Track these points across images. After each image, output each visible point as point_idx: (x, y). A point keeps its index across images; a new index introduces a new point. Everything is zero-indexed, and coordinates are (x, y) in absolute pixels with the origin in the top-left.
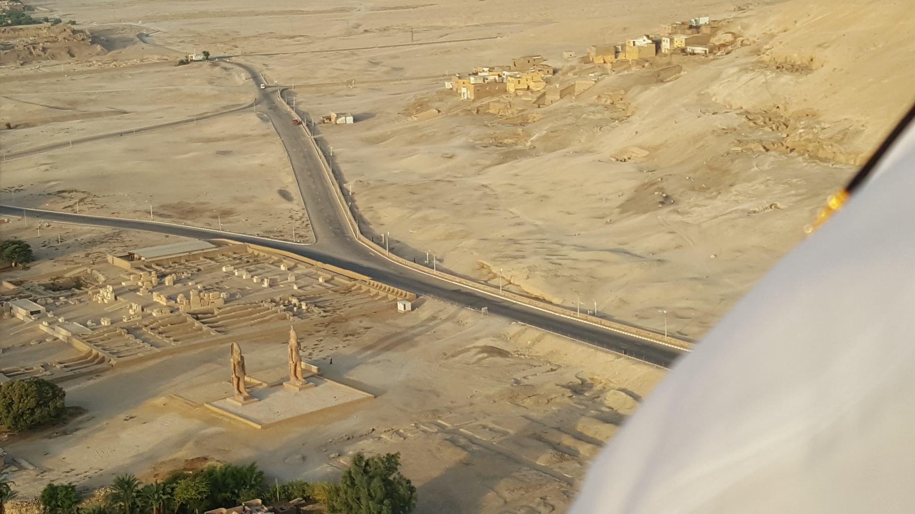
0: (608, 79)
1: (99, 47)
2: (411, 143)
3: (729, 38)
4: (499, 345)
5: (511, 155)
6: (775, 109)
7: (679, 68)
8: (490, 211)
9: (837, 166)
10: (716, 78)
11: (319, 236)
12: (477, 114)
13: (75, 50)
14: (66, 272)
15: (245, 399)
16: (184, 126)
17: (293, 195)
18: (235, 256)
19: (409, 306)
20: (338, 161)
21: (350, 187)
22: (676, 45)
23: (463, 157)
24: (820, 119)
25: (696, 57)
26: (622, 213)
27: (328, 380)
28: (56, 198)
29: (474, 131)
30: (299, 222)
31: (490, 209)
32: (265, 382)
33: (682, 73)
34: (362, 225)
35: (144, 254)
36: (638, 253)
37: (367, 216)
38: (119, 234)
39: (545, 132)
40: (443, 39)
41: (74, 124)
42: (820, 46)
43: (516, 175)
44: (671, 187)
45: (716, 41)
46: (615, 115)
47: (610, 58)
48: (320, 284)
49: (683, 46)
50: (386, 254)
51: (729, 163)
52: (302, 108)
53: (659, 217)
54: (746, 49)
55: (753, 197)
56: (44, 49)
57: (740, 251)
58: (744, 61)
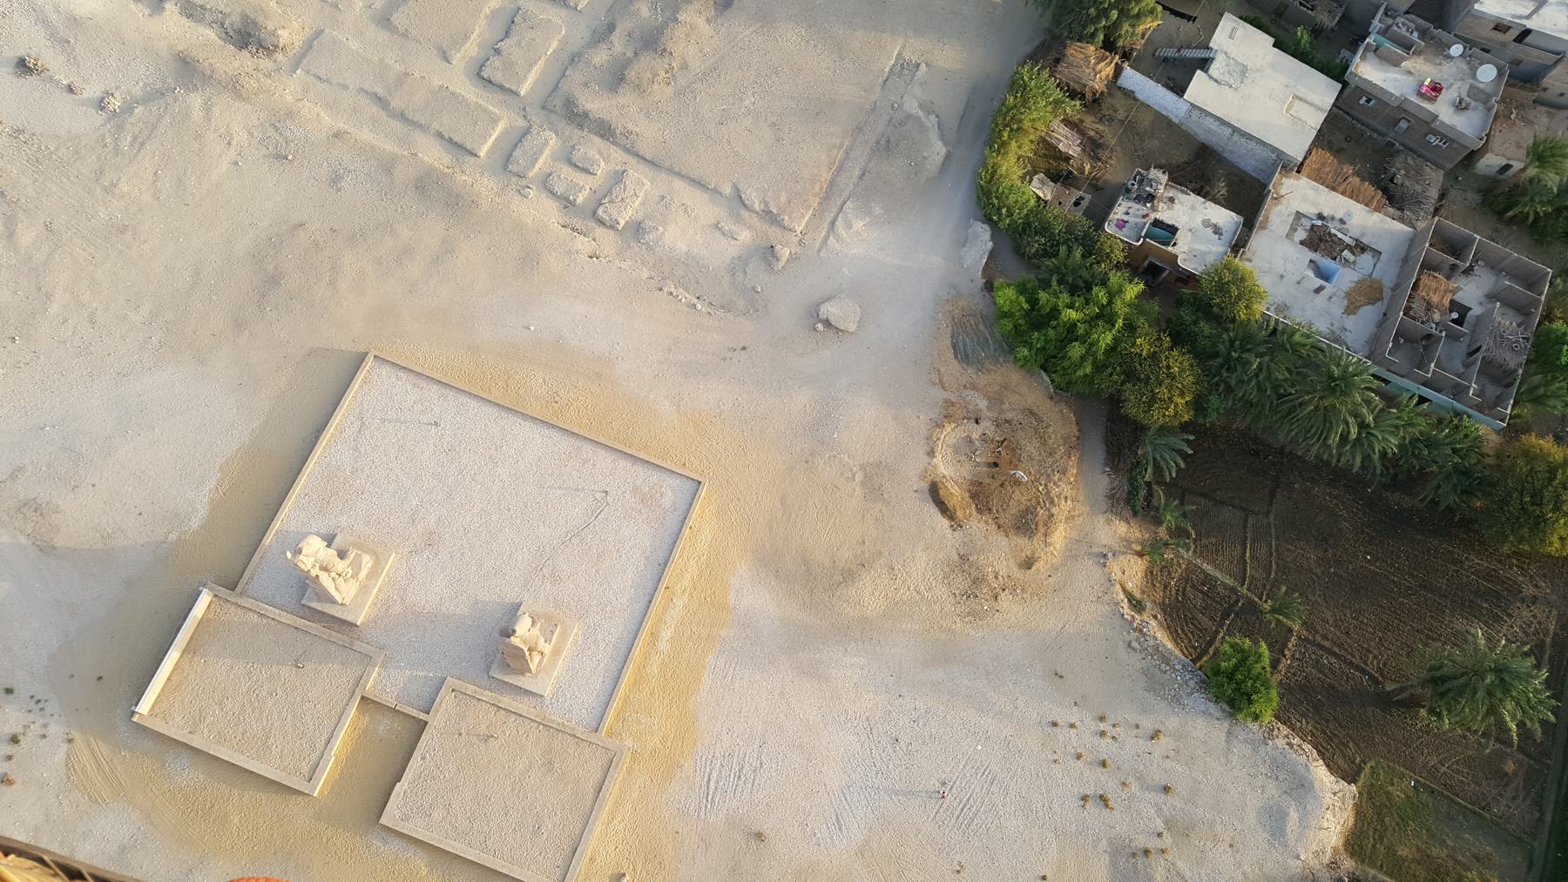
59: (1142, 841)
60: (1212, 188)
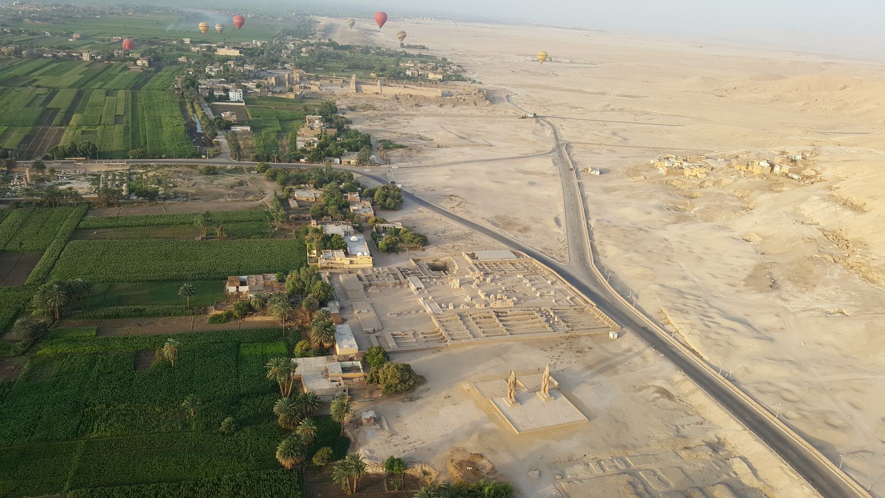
0: (741, 181)
1: (488, 102)
2: (628, 197)
3: (813, 173)
4: (668, 388)
5: (682, 218)
6: (839, 231)
7: (782, 185)
8: (668, 262)
9: (880, 288)
10: (804, 200)
11: (571, 259)
12: (666, 186)
13: (477, 102)
14: (441, 257)
16: (517, 160)
17: (563, 224)
18: (525, 265)
20: (588, 201)
21: (592, 223)
22: (783, 170)
23: (656, 214)
24: (871, 251)
25: (793, 181)
26: (746, 285)
27: (563, 396)
28: (447, 200)
29: (662, 198)
30: (562, 245)
31: (668, 260)
33: (784, 188)
34: (596, 256)
35: (482, 256)
36: (756, 327)
37: (599, 248)
38: (471, 234)
39: (703, 207)
40: (649, 122)
41: (467, 150)
42: (871, 197)
43: (684, 235)
44: (777, 273)
45: (805, 172)
46: (743, 205)
47: (744, 168)
48: (567, 301)
49: (787, 172)
50: (606, 284)
51: (813, 266)
52: (575, 158)
53: (770, 299)
54: (823, 184)
55: (828, 299)
56: (464, 100)
57: (820, 344)
58: (823, 192)
59: (394, 437)
60: (182, 49)
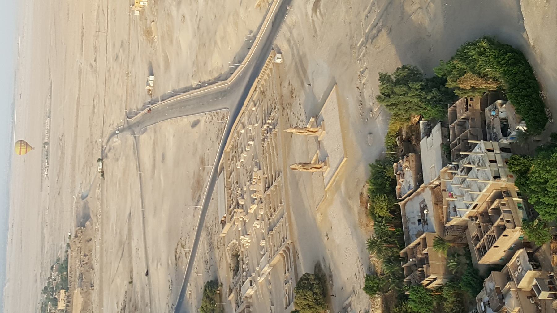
15: (325, 165)
19: (279, 56)
32: (317, 151)
